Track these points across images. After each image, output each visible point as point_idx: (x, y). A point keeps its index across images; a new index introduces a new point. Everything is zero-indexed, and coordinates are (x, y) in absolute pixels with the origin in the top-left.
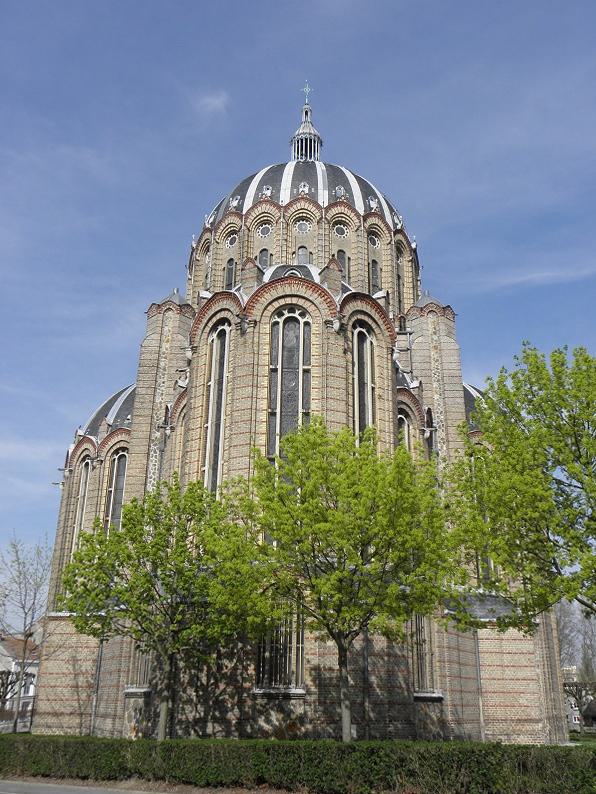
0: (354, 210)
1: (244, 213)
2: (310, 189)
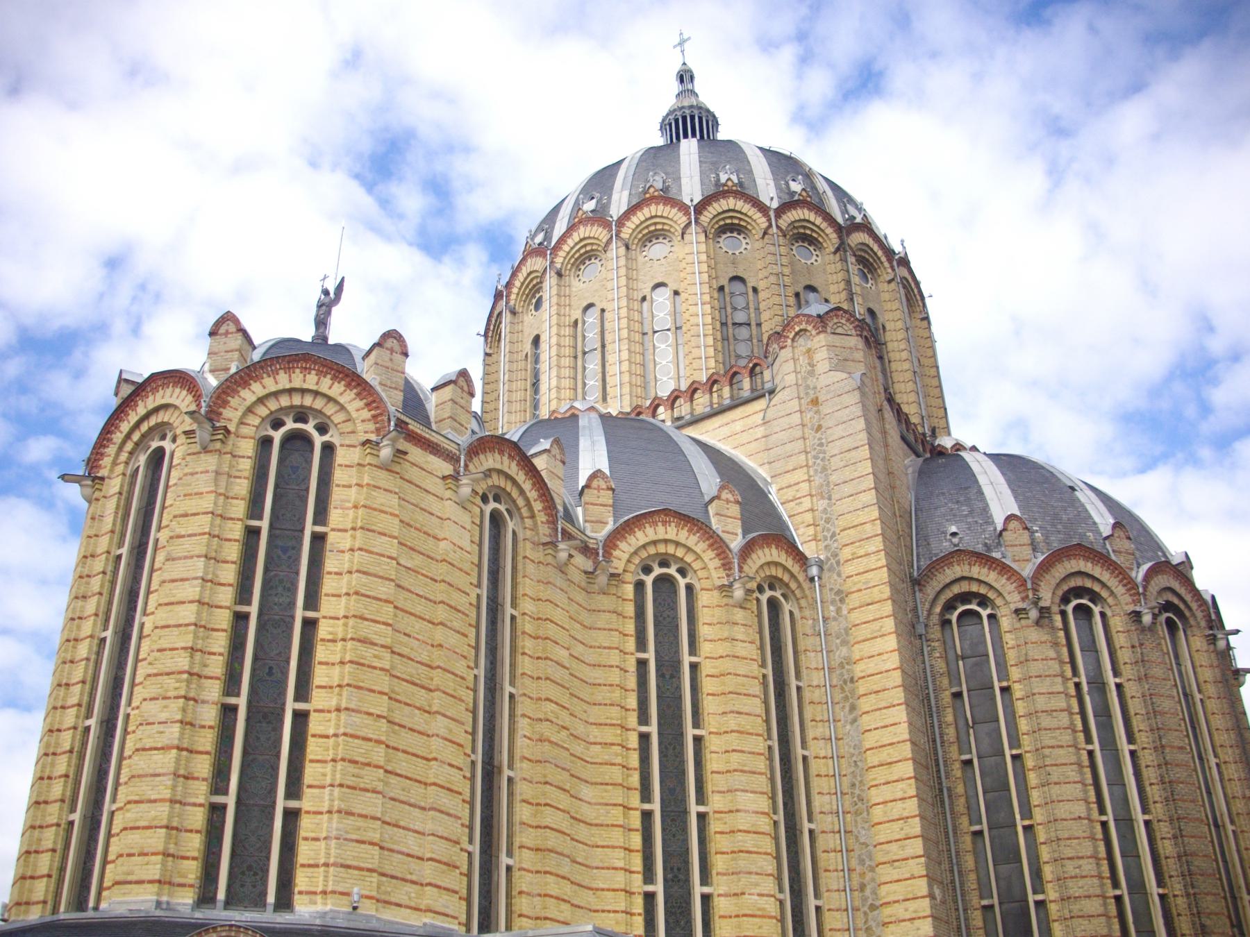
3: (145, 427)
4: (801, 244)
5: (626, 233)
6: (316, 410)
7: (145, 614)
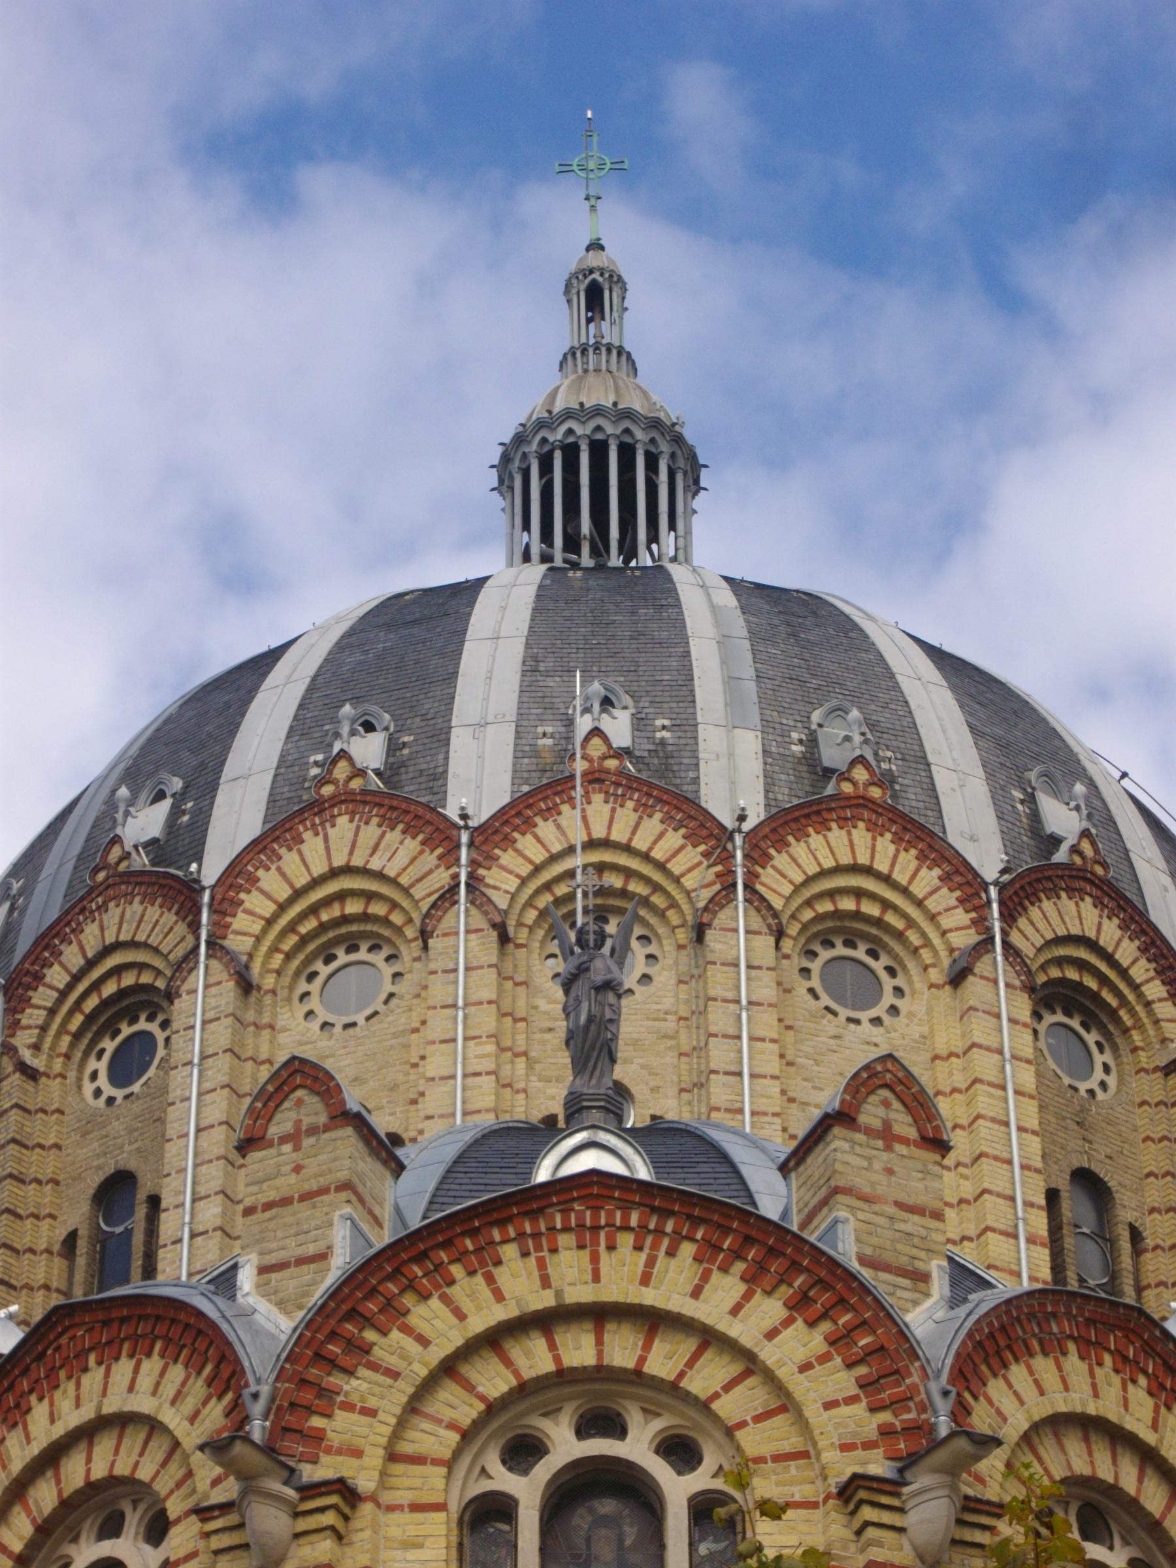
1: (211, 869)
2: (640, 723)
4: (1060, 1017)
6: (655, 1383)
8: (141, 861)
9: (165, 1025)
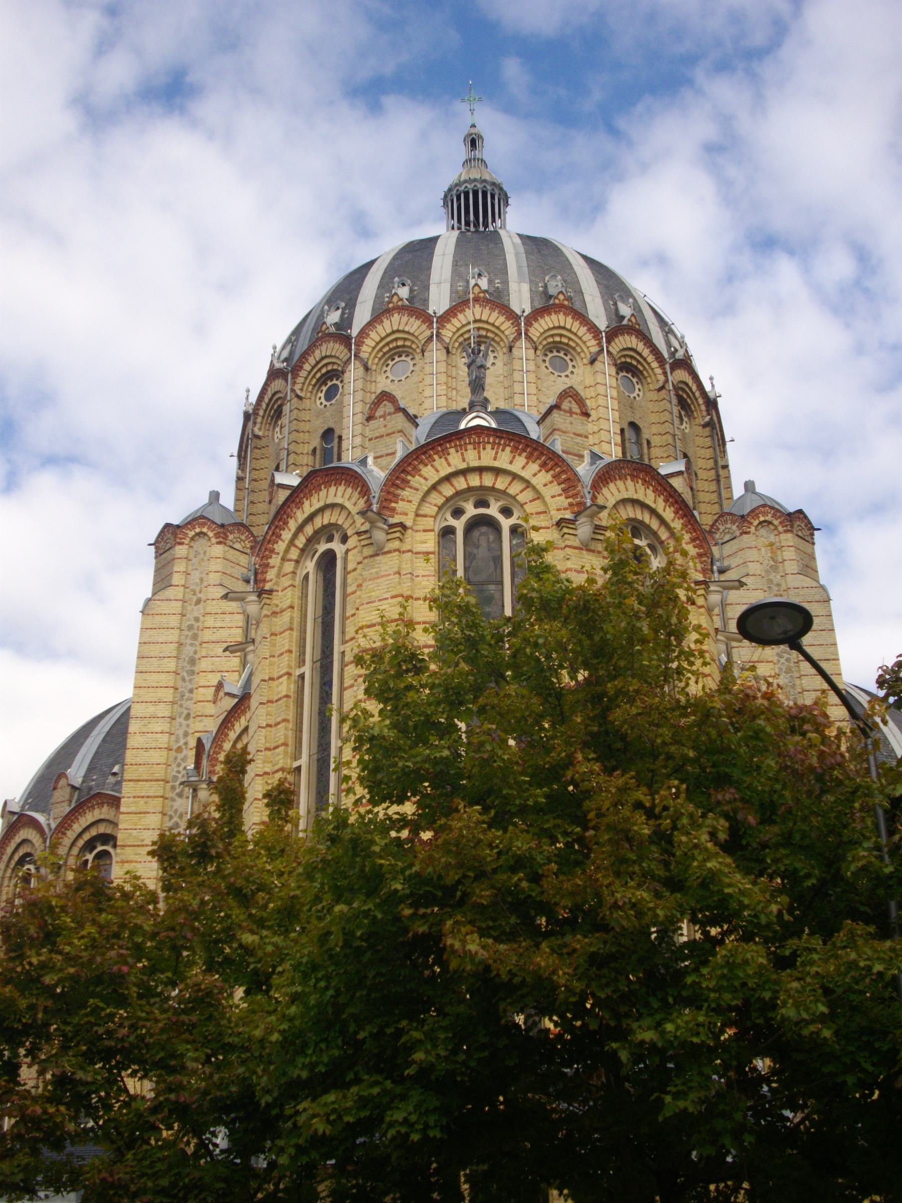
0: (582, 317)
1: (355, 332)
3: (309, 530)
5: (447, 333)
7: (344, 642)
8: (333, 330)
9: (342, 382)
